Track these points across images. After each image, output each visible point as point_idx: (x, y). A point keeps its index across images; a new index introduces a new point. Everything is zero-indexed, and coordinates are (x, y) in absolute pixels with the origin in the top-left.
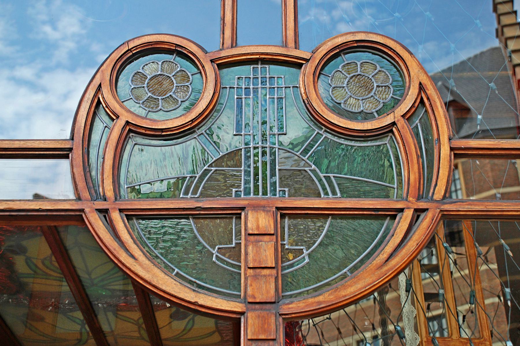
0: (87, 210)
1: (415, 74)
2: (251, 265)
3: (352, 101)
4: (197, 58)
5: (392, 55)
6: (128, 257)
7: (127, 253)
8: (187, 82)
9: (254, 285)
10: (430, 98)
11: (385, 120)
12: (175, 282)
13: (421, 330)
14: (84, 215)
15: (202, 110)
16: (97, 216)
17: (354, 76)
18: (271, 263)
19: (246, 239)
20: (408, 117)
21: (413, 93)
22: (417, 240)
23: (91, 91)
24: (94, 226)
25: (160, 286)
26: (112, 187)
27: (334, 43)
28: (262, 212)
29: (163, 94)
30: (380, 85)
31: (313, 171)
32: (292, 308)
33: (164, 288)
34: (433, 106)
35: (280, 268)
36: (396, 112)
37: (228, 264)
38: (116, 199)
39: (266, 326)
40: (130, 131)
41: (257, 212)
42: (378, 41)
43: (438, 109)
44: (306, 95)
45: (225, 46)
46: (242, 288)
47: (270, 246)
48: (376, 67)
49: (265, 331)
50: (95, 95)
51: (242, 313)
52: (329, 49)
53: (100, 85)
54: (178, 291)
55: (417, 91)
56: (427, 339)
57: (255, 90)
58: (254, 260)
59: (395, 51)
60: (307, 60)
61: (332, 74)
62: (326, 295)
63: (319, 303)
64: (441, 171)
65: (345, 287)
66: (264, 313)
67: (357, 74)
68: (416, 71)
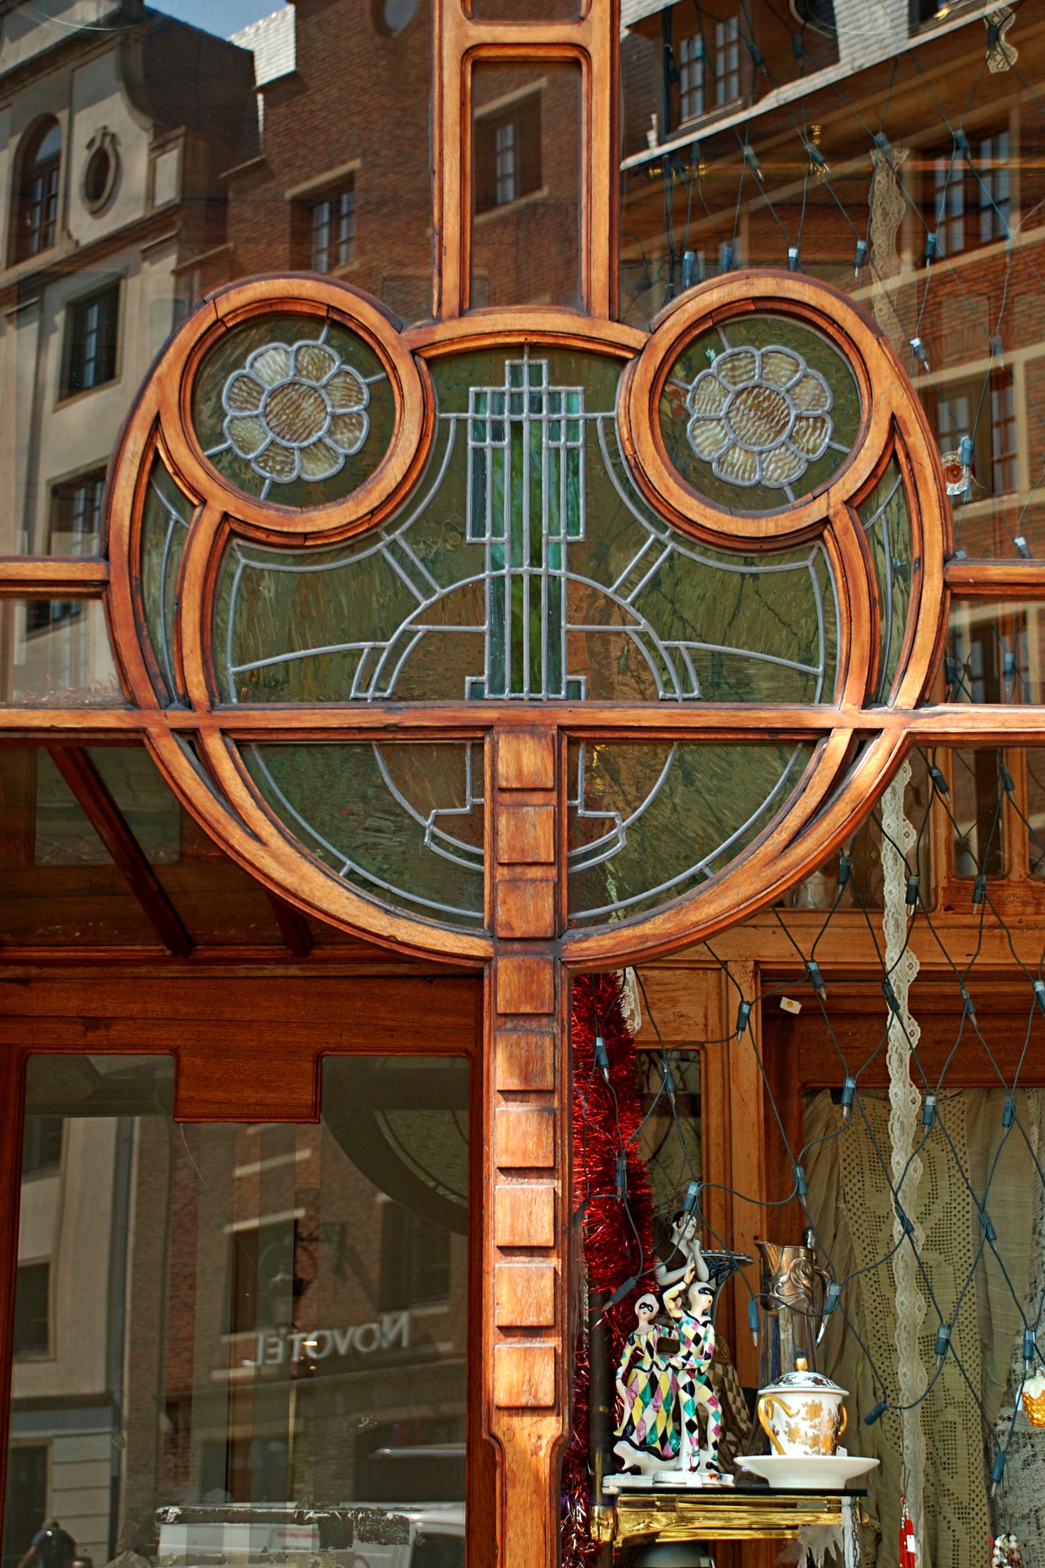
0: (153, 730)
1: (883, 393)
2: (504, 859)
3: (737, 456)
4: (379, 343)
5: (836, 335)
6: (248, 838)
7: (244, 830)
8: (357, 403)
9: (511, 901)
10: (912, 455)
11: (806, 513)
12: (347, 894)
13: (936, 860)
14: (146, 741)
15: (394, 485)
16: (175, 744)
17: (744, 389)
18: (547, 854)
19: (494, 800)
20: (860, 503)
21: (873, 443)
22: (853, 801)
23: (139, 433)
24: (171, 769)
25: (317, 903)
26: (202, 677)
27: (701, 305)
28: (528, 738)
29: (304, 435)
30: (806, 413)
31: (643, 635)
32: (588, 949)
33: (325, 906)
34: (917, 475)
35: (565, 862)
36: (832, 490)
37: (457, 851)
38: (212, 704)
39: (534, 987)
40: (233, 533)
41: (518, 738)
42: (806, 299)
43: (926, 483)
44: (633, 445)
45: (445, 310)
46: (486, 907)
47: (544, 817)
48: (798, 365)
49: (532, 997)
50: (149, 444)
51: (486, 960)
52: (689, 323)
53: (157, 419)
54: (355, 912)
55: (884, 437)
56: (949, 881)
57: (517, 427)
58: (512, 848)
59: (842, 328)
60: (638, 353)
61: (695, 383)
62: (659, 920)
63: (644, 938)
64: (918, 640)
65: (697, 905)
66: (529, 960)
67: (751, 383)
68: (886, 383)
